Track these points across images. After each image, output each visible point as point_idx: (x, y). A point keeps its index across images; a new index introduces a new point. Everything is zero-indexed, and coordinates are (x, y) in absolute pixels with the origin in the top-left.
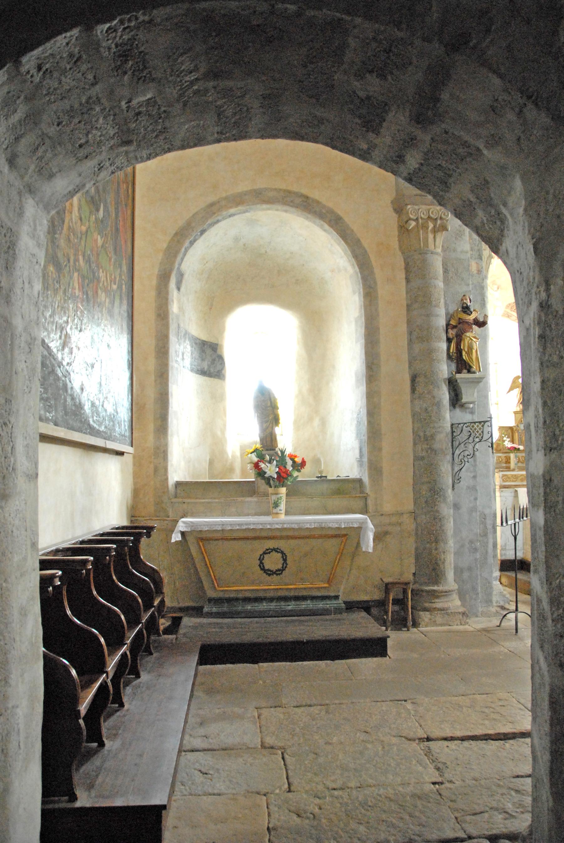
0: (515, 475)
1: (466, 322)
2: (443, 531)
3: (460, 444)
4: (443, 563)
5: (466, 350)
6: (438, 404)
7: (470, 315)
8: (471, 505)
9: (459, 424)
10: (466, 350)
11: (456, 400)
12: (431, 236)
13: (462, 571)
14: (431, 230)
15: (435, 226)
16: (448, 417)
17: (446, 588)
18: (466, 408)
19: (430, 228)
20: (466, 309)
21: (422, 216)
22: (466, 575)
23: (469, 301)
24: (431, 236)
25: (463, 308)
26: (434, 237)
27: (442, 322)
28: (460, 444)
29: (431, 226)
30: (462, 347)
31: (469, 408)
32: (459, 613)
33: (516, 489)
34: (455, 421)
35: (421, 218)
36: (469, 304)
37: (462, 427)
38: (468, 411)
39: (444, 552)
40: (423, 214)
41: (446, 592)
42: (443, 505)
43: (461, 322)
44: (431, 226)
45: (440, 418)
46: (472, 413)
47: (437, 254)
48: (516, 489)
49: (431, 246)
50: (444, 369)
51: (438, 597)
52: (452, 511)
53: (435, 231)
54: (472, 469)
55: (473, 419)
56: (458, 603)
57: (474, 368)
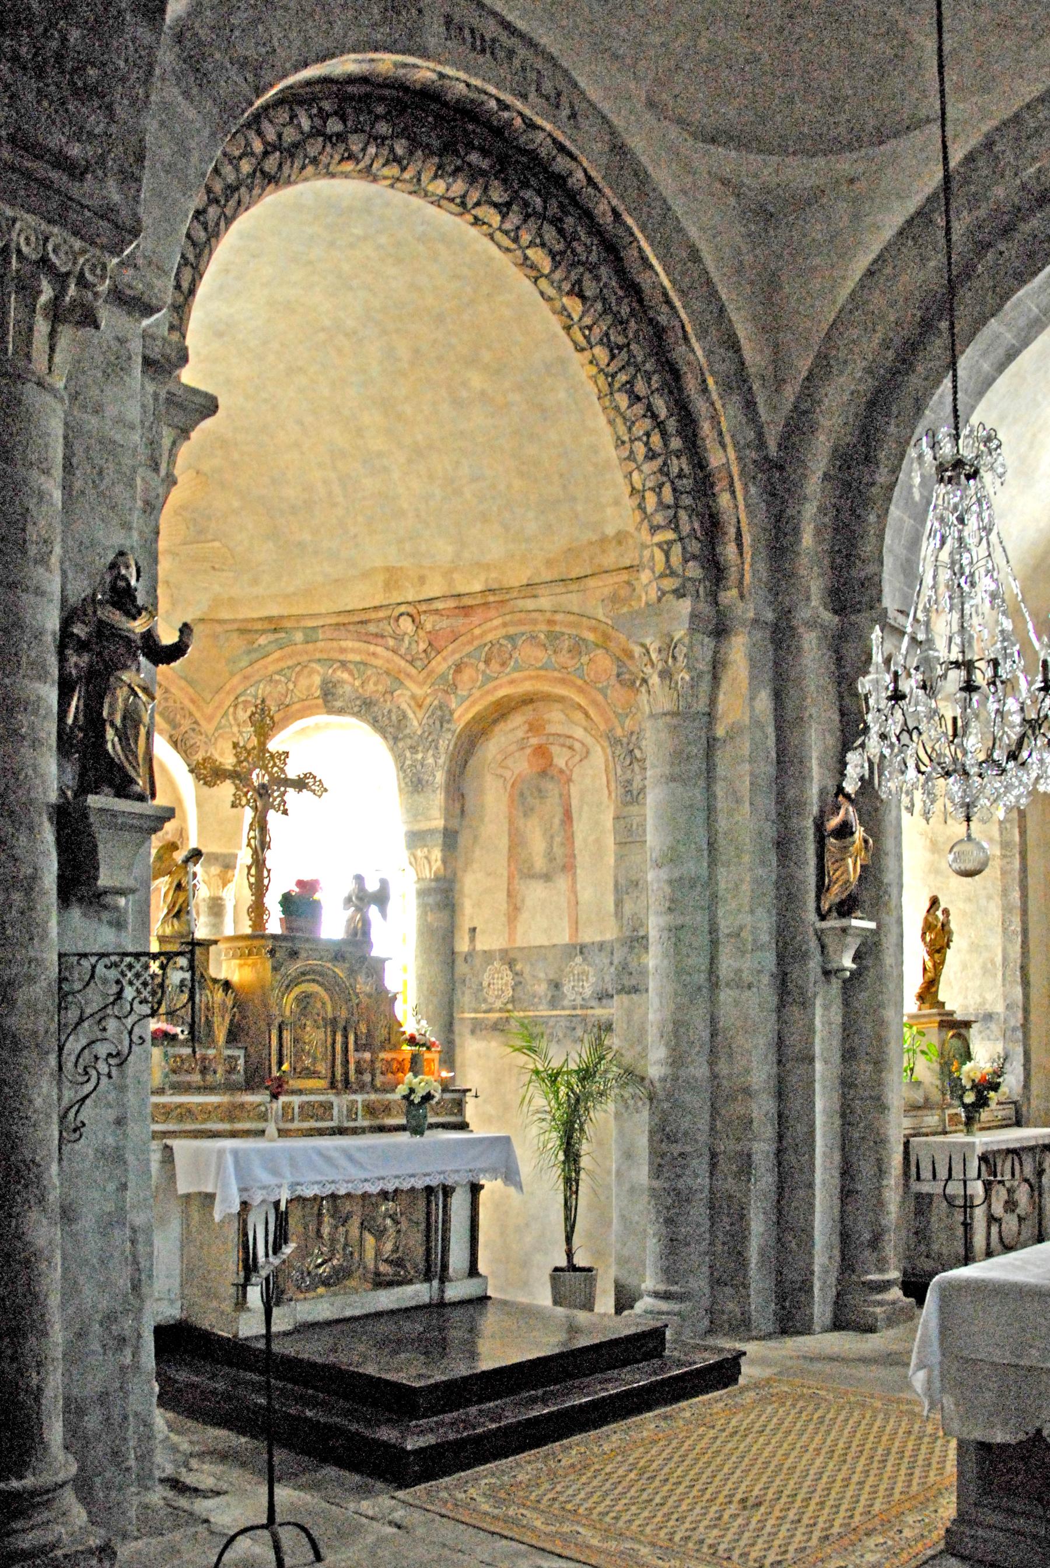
0: (164, 1106)
1: (121, 637)
2: (36, 1296)
3: (82, 1020)
4: (37, 1400)
5: (118, 722)
6: (30, 885)
7: (135, 619)
8: (110, 1207)
9: (85, 955)
10: (118, 722)
11: (78, 882)
12: (42, 327)
13: (81, 1412)
14: (45, 307)
15: (57, 299)
16: (57, 930)
17: (46, 1479)
18: (105, 907)
19: (43, 299)
20: (123, 598)
21: (25, 249)
22: (92, 1422)
23: (133, 570)
24: (42, 327)
25: (114, 588)
26: (52, 334)
27: (52, 621)
28: (82, 1020)
29: (47, 294)
30: (105, 714)
31: (117, 908)
32: (91, 1552)
33: (169, 1142)
34: (67, 948)
35: (19, 251)
36: (133, 582)
37: (94, 967)
38: (105, 916)
39: (39, 1364)
40: (27, 239)
41: (48, 1491)
42: (34, 1215)
43: (104, 631)
44: (47, 294)
45: (33, 932)
46: (119, 925)
47: (52, 390)
48: (169, 1142)
49: (39, 363)
50: (49, 775)
51: (21, 1513)
52: (57, 1233)
53: (57, 314)
54: (112, 1096)
55: (120, 946)
56: (79, 1515)
57: (141, 784)
